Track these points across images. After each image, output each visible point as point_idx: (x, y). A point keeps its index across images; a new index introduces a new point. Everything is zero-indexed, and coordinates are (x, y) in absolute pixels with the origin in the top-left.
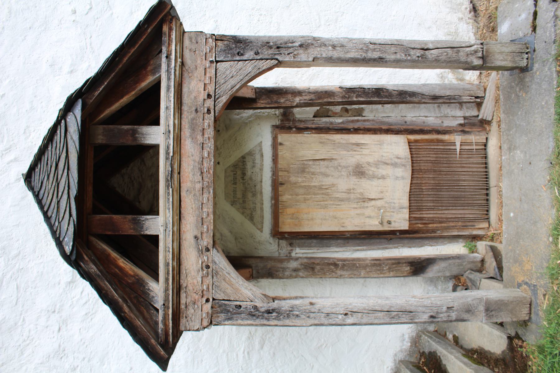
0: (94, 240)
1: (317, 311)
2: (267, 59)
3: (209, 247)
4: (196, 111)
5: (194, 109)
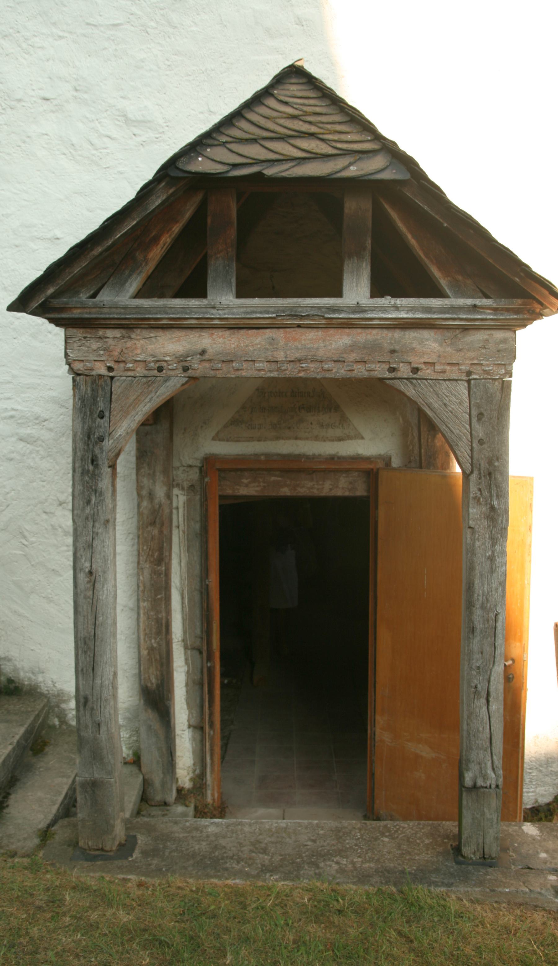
0: (198, 198)
1: (96, 530)
2: (472, 458)
3: (190, 371)
4: (393, 352)
5: (397, 348)
